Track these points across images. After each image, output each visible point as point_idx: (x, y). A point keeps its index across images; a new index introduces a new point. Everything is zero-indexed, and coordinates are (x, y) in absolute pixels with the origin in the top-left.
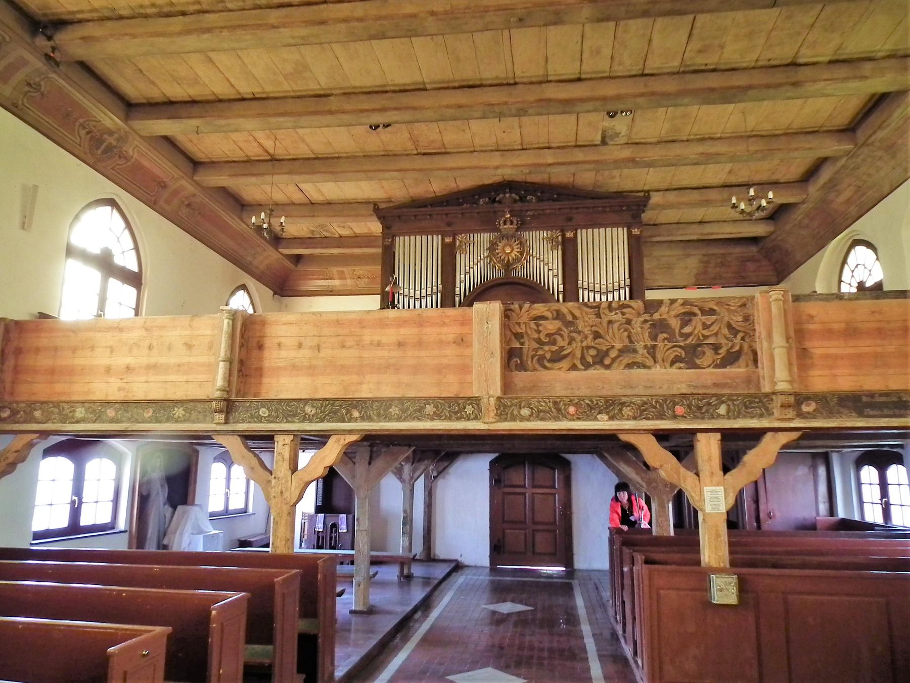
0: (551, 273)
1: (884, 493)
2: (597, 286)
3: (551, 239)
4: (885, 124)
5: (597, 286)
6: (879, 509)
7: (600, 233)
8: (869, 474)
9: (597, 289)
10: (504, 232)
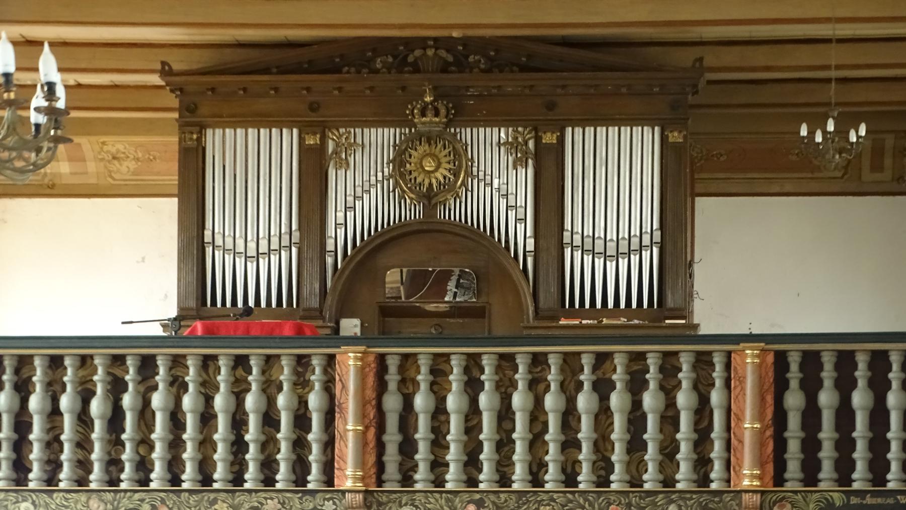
0: (512, 214)
3: (513, 146)
7: (609, 137)
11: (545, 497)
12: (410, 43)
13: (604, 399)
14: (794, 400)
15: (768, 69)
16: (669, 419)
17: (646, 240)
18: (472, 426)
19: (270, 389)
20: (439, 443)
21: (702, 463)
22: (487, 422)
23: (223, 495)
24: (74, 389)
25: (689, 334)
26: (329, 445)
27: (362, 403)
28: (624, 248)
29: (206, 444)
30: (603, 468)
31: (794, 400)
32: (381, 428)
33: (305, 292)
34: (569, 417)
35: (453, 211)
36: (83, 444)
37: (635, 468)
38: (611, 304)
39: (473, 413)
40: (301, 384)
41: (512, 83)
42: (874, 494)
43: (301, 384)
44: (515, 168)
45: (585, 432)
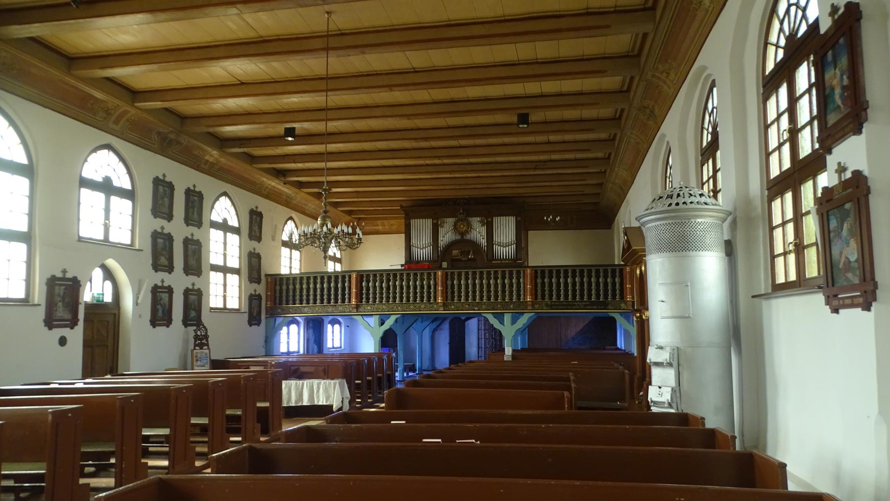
3: (481, 222)
4: (827, 91)
12: (457, 199)
14: (539, 281)
16: (511, 285)
19: (422, 280)
20: (460, 292)
21: (519, 295)
26: (435, 292)
27: (442, 283)
29: (408, 293)
31: (539, 281)
32: (447, 288)
34: (489, 285)
35: (468, 237)
36: (381, 293)
43: (429, 279)
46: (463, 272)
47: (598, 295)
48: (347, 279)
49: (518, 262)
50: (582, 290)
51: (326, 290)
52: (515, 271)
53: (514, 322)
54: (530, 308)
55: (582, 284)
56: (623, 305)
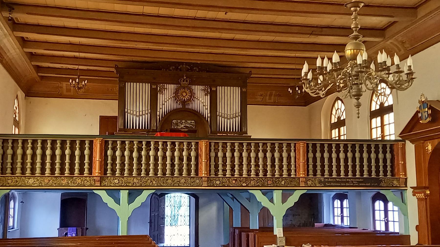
0: (204, 107)
1: (386, 215)
2: (226, 115)
5: (226, 115)
6: (383, 224)
7: (228, 89)
8: (337, 203)
9: (226, 116)
10: (182, 85)
11: (252, 179)
13: (114, 152)
14: (311, 155)
15: (262, 74)
16: (281, 160)
17: (237, 115)
18: (233, 161)
20: (224, 165)
21: (289, 170)
22: (269, 160)
23: (170, 178)
24: (145, 150)
25: (249, 138)
27: (206, 154)
28: (232, 117)
29: (164, 165)
30: (265, 171)
33: (152, 125)
34: (257, 158)
35: (190, 107)
37: (273, 172)
38: (228, 130)
39: (233, 157)
40: (189, 149)
41: (205, 75)
42: (331, 178)
44: (205, 95)
45: (261, 162)
46: (221, 143)
47: (370, 172)
48: (87, 145)
49: (241, 133)
50: (354, 166)
51: (67, 157)
52: (221, 143)
53: (284, 201)
54: (302, 184)
55: (354, 159)
56: (395, 182)
